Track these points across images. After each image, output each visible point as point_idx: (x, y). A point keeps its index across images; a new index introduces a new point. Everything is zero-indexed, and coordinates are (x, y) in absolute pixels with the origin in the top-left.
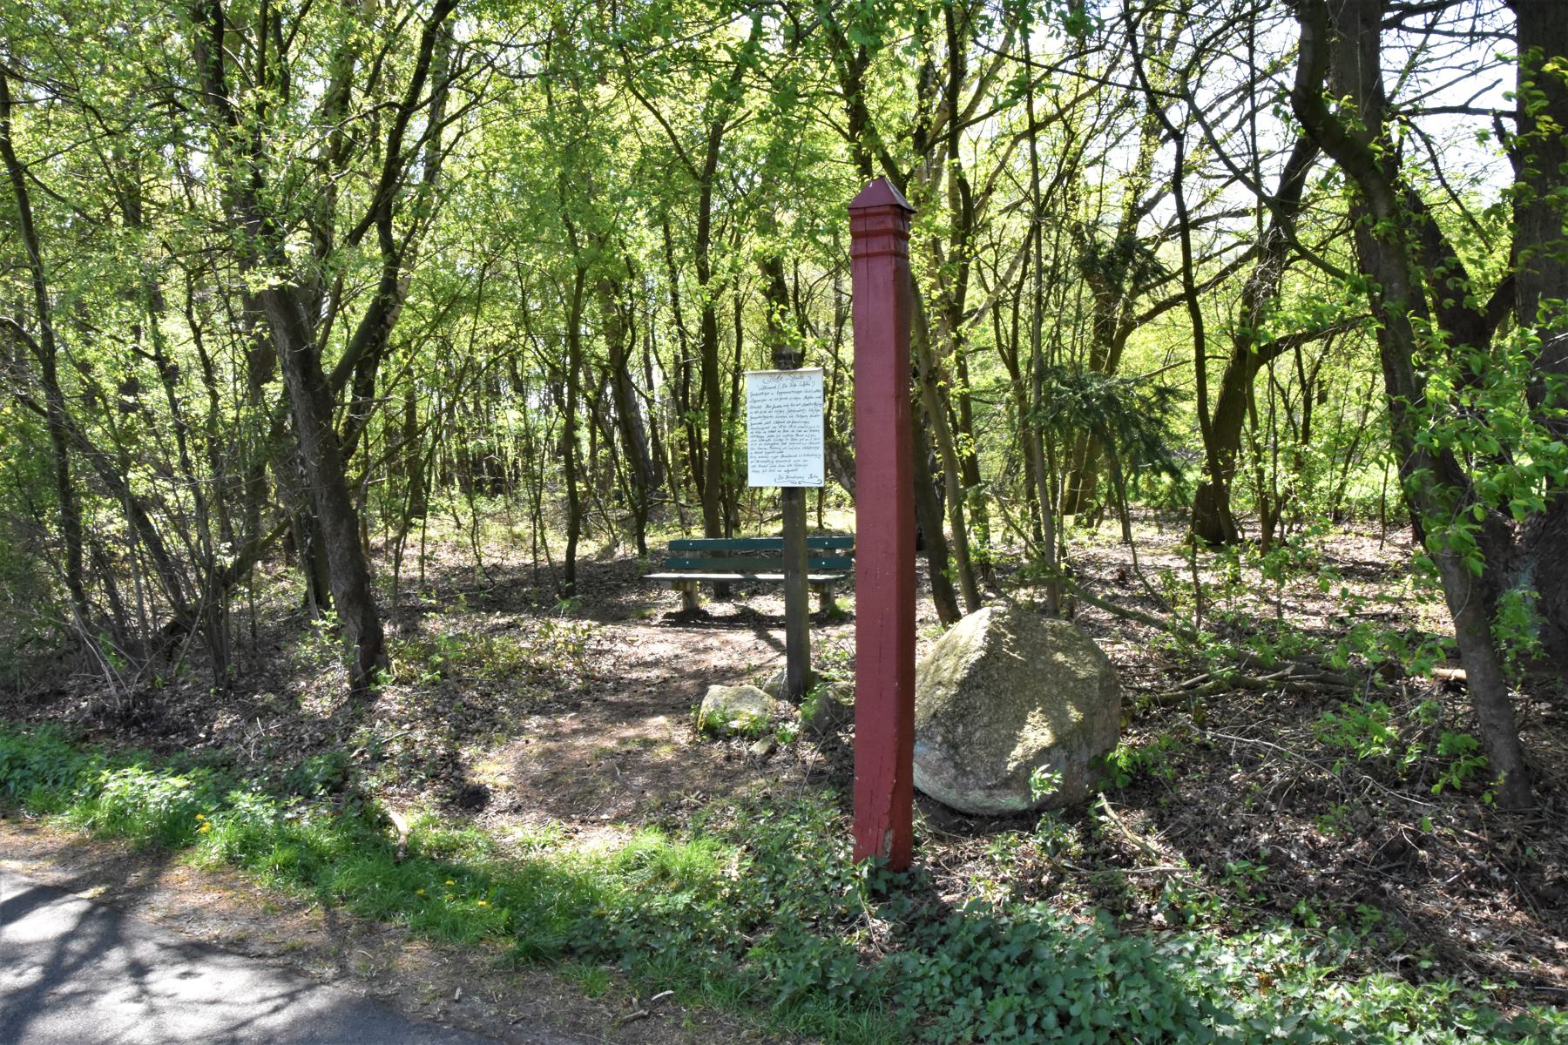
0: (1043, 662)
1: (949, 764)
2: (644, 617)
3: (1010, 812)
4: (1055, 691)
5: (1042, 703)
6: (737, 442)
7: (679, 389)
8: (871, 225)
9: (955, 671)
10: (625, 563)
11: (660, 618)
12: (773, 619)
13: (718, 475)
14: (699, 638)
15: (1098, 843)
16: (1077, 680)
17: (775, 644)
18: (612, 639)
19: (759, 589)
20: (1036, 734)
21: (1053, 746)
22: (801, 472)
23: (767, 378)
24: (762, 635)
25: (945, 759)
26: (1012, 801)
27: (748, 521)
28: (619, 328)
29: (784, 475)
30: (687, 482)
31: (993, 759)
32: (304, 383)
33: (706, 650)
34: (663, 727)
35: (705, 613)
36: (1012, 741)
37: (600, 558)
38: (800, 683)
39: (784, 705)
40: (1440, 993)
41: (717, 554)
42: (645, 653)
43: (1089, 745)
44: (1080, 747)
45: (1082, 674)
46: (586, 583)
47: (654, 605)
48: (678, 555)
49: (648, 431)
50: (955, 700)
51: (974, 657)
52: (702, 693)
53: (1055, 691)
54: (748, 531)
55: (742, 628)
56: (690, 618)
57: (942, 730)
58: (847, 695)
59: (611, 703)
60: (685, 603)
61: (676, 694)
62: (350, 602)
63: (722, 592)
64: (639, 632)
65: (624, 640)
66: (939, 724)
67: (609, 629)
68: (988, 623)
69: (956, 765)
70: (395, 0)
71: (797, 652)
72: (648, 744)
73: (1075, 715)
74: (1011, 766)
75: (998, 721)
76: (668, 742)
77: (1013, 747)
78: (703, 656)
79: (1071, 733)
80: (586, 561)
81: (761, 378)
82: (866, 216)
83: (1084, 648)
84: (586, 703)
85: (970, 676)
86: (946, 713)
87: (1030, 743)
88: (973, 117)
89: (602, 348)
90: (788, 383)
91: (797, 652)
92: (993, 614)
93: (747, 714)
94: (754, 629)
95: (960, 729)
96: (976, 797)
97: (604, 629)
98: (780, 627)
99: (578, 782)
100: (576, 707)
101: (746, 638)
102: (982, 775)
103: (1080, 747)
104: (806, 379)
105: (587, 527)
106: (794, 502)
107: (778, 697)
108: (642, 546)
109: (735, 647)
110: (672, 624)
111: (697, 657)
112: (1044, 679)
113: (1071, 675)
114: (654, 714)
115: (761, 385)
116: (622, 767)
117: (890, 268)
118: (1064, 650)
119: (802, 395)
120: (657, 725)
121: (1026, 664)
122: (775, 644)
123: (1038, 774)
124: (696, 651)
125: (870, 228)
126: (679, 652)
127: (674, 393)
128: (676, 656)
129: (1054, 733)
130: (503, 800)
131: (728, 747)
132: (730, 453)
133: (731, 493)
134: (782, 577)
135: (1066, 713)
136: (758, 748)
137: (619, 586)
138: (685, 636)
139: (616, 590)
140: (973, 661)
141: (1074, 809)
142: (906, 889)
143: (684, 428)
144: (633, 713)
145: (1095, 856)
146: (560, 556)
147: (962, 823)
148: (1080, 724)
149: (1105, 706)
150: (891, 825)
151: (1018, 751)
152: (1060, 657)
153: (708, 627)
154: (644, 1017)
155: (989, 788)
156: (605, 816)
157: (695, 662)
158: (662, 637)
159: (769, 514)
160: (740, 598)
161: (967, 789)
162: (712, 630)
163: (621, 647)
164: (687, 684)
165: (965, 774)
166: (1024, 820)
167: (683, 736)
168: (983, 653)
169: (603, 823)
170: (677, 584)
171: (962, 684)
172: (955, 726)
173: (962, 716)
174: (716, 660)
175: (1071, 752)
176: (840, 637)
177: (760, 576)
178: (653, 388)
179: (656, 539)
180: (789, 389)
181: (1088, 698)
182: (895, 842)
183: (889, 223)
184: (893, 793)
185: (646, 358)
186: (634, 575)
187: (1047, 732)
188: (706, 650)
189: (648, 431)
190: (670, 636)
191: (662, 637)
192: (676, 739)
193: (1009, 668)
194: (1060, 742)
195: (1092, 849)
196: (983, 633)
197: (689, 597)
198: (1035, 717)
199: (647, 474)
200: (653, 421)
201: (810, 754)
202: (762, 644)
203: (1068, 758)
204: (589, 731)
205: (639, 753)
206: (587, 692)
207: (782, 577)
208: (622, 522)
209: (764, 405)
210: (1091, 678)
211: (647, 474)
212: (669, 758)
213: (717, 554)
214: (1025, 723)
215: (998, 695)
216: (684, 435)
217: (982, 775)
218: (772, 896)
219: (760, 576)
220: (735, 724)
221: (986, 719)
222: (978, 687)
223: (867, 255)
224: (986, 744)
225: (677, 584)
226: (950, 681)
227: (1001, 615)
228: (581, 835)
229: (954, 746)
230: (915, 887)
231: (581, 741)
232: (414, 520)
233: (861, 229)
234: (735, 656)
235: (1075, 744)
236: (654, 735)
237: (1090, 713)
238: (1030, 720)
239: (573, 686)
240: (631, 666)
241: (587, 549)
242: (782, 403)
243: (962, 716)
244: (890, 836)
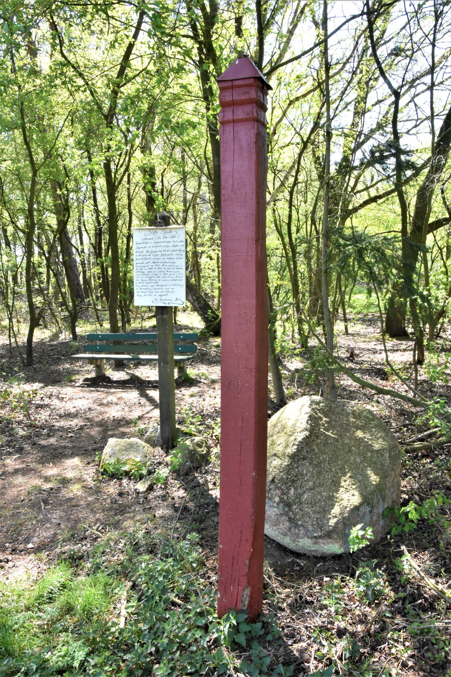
0: (350, 438)
2: (71, 381)
3: (330, 555)
4: (358, 460)
5: (351, 469)
6: (128, 275)
7: (97, 247)
8: (238, 96)
9: (287, 446)
10: (64, 344)
11: (81, 382)
12: (149, 382)
13: (117, 290)
14: (103, 395)
15: (404, 587)
16: (373, 451)
17: (151, 400)
18: (50, 397)
19: (139, 363)
20: (349, 497)
21: (361, 504)
23: (147, 232)
24: (143, 395)
25: (281, 514)
26: (334, 548)
27: (135, 318)
28: (63, 210)
30: (102, 297)
31: (317, 516)
33: (108, 404)
34: (74, 468)
35: (109, 378)
36: (331, 501)
37: (51, 340)
38: (169, 439)
39: (159, 451)
40: (45, 196)
41: (117, 343)
42: (70, 407)
43: (384, 500)
44: (378, 502)
45: (377, 446)
46: (40, 356)
47: (78, 373)
48: (92, 342)
49: (80, 269)
50: (288, 469)
51: (300, 436)
52: (104, 441)
53: (358, 460)
54: (135, 325)
55: (131, 388)
56: (100, 381)
57: (278, 492)
58: (201, 446)
59: (44, 447)
60: (97, 372)
61: (87, 441)
63: (119, 365)
64: (67, 391)
65: (58, 397)
66: (277, 488)
67: (51, 389)
68: (309, 410)
71: (167, 408)
72: (65, 482)
73: (374, 478)
74: (332, 522)
75: (320, 485)
76: (80, 480)
77: (333, 506)
78: (106, 409)
79: (372, 493)
80: (42, 343)
81: (143, 232)
83: (376, 426)
84: (27, 447)
85: (298, 450)
86: (282, 478)
87: (345, 503)
88: (284, 60)
89: (52, 220)
90: (162, 236)
91: (167, 408)
92: (313, 402)
93: (133, 460)
94: (137, 388)
95: (292, 491)
96: (305, 544)
97: (46, 389)
98: (155, 387)
99: (13, 515)
100: (20, 450)
101: (133, 395)
102: (310, 528)
103: (378, 502)
104: (174, 233)
105: (44, 322)
106: (165, 316)
107: (154, 445)
108: (74, 332)
109: (124, 404)
110: (89, 386)
111: (103, 409)
112: (350, 451)
113: (369, 447)
114: (72, 455)
115: (143, 237)
116: (46, 502)
117: (252, 133)
118: (363, 428)
119: (171, 244)
120: (73, 466)
121: (337, 440)
122: (151, 400)
123: (356, 531)
124: (101, 404)
125: (236, 97)
126: (91, 406)
127: (94, 248)
128: (90, 409)
129: (361, 494)
131: (120, 485)
132: (125, 281)
133: (125, 303)
134: (156, 357)
135: (367, 477)
136: (142, 487)
137: (59, 359)
138: (95, 395)
139: (58, 361)
140: (300, 439)
141: (382, 553)
142: (262, 640)
143: (99, 267)
144: (56, 455)
145: (404, 599)
146: (23, 339)
147: (298, 566)
148: (378, 485)
149: (393, 470)
150: (249, 583)
151: (336, 510)
152: (359, 434)
153: (110, 387)
155: (316, 537)
156: (30, 546)
157: (101, 413)
158: (81, 395)
159: (147, 315)
160: (130, 368)
161: (298, 537)
162: (113, 390)
163: (55, 402)
164: (95, 432)
165: (297, 526)
166: (345, 564)
167: (90, 474)
168: (307, 433)
169: (28, 552)
170: (91, 361)
171: (293, 457)
172: (289, 489)
173: (293, 481)
174: (114, 413)
175: (372, 507)
176: (192, 396)
177: (142, 357)
178: (83, 244)
179: (83, 329)
180: (161, 240)
181: (382, 464)
182: (251, 597)
183: (253, 94)
184: (251, 560)
185: (80, 228)
186: (65, 352)
187: (356, 493)
188: (108, 404)
189: (80, 269)
190: (87, 395)
191: (81, 395)
192: (86, 477)
193: (326, 444)
194: (366, 501)
195: (401, 595)
196: (306, 417)
197: (99, 368)
198: (346, 482)
199: (79, 292)
200: (83, 263)
201: (179, 493)
202: (143, 401)
203: (371, 512)
204: (25, 472)
205: (58, 490)
206: (29, 437)
207: (156, 357)
208: (64, 319)
209: (145, 250)
210: (383, 450)
211: (79, 292)
212: (80, 493)
213: (117, 343)
214: (340, 486)
215: (318, 465)
216: (99, 271)
217: (310, 528)
218: (153, 644)
219: (142, 357)
220: (126, 468)
221: (311, 483)
222: (304, 459)
223: (234, 121)
224: (312, 504)
225: (91, 361)
226: (284, 454)
227: (318, 403)
228: (10, 564)
229: (288, 505)
230: (269, 637)
231: (19, 480)
233: (228, 98)
234: (126, 409)
235: (375, 500)
236: (70, 475)
237: (383, 474)
238: (343, 484)
239: (21, 433)
240: (60, 416)
241: (40, 335)
242: (158, 249)
243: (293, 481)
244: (247, 592)
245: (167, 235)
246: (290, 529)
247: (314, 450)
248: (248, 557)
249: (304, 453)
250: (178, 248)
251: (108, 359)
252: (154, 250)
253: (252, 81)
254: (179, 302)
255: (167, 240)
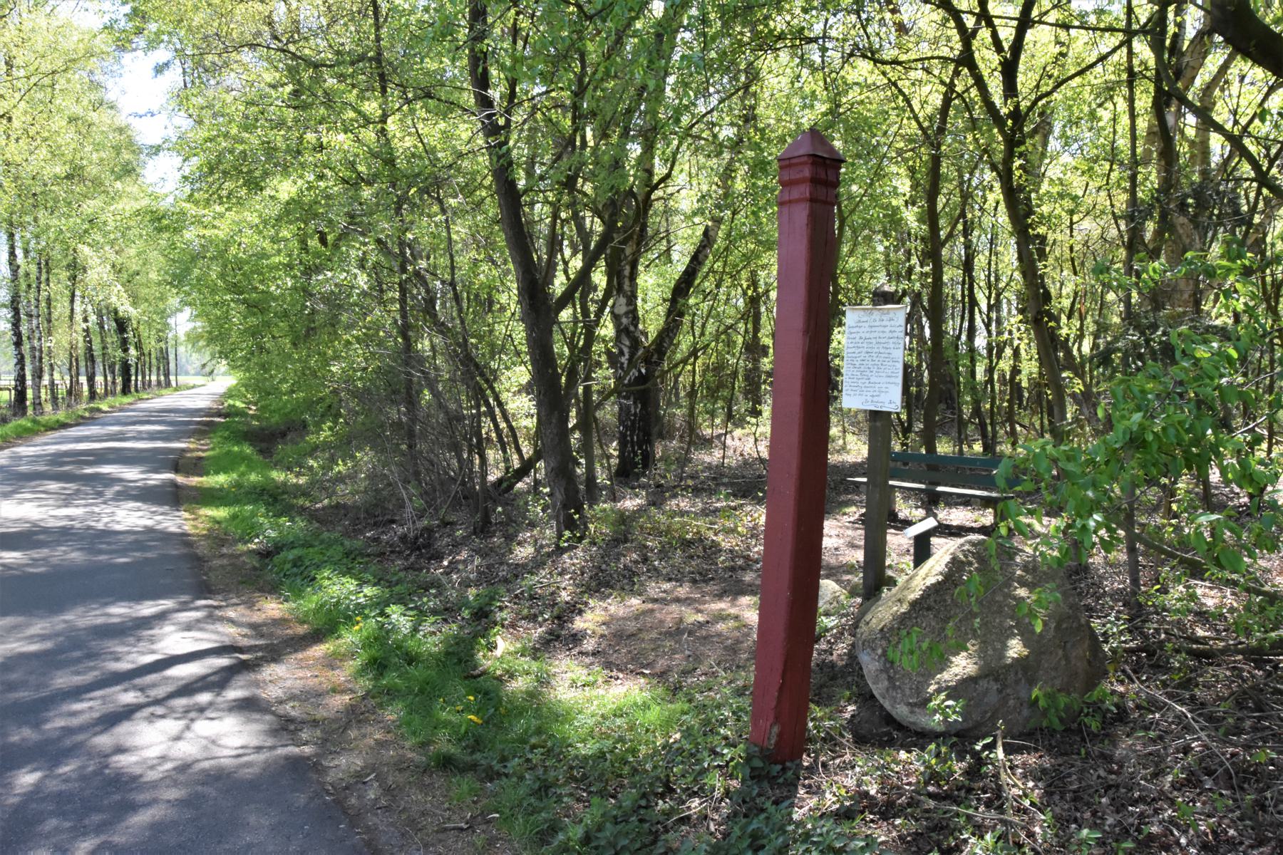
1: (884, 676)
22: (883, 398)
23: (862, 313)
29: (869, 399)
32: (530, 305)
62: (557, 475)
69: (890, 679)
70: (1005, 9)
77: (942, 671)
82: (790, 166)
90: (878, 318)
102: (908, 692)
104: (891, 315)
115: (857, 319)
119: (887, 330)
130: (589, 645)
148: (1018, 661)
150: (777, 719)
154: (462, 829)
165: (894, 688)
168: (940, 578)
175: (1005, 686)
180: (878, 323)
182: (780, 735)
217: (908, 692)
222: (929, 609)
223: (790, 202)
232: (748, 419)
233: (786, 178)
244: (776, 730)
245: (884, 317)
246: (887, 690)
247: (945, 601)
248: (777, 688)
249: (931, 601)
250: (895, 335)
251: (901, 487)
252: (868, 335)
253: (805, 159)
254: (893, 406)
255: (884, 323)
